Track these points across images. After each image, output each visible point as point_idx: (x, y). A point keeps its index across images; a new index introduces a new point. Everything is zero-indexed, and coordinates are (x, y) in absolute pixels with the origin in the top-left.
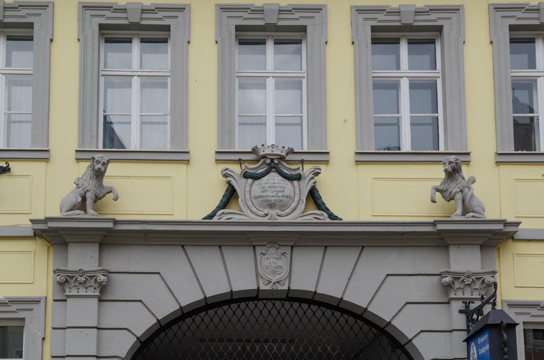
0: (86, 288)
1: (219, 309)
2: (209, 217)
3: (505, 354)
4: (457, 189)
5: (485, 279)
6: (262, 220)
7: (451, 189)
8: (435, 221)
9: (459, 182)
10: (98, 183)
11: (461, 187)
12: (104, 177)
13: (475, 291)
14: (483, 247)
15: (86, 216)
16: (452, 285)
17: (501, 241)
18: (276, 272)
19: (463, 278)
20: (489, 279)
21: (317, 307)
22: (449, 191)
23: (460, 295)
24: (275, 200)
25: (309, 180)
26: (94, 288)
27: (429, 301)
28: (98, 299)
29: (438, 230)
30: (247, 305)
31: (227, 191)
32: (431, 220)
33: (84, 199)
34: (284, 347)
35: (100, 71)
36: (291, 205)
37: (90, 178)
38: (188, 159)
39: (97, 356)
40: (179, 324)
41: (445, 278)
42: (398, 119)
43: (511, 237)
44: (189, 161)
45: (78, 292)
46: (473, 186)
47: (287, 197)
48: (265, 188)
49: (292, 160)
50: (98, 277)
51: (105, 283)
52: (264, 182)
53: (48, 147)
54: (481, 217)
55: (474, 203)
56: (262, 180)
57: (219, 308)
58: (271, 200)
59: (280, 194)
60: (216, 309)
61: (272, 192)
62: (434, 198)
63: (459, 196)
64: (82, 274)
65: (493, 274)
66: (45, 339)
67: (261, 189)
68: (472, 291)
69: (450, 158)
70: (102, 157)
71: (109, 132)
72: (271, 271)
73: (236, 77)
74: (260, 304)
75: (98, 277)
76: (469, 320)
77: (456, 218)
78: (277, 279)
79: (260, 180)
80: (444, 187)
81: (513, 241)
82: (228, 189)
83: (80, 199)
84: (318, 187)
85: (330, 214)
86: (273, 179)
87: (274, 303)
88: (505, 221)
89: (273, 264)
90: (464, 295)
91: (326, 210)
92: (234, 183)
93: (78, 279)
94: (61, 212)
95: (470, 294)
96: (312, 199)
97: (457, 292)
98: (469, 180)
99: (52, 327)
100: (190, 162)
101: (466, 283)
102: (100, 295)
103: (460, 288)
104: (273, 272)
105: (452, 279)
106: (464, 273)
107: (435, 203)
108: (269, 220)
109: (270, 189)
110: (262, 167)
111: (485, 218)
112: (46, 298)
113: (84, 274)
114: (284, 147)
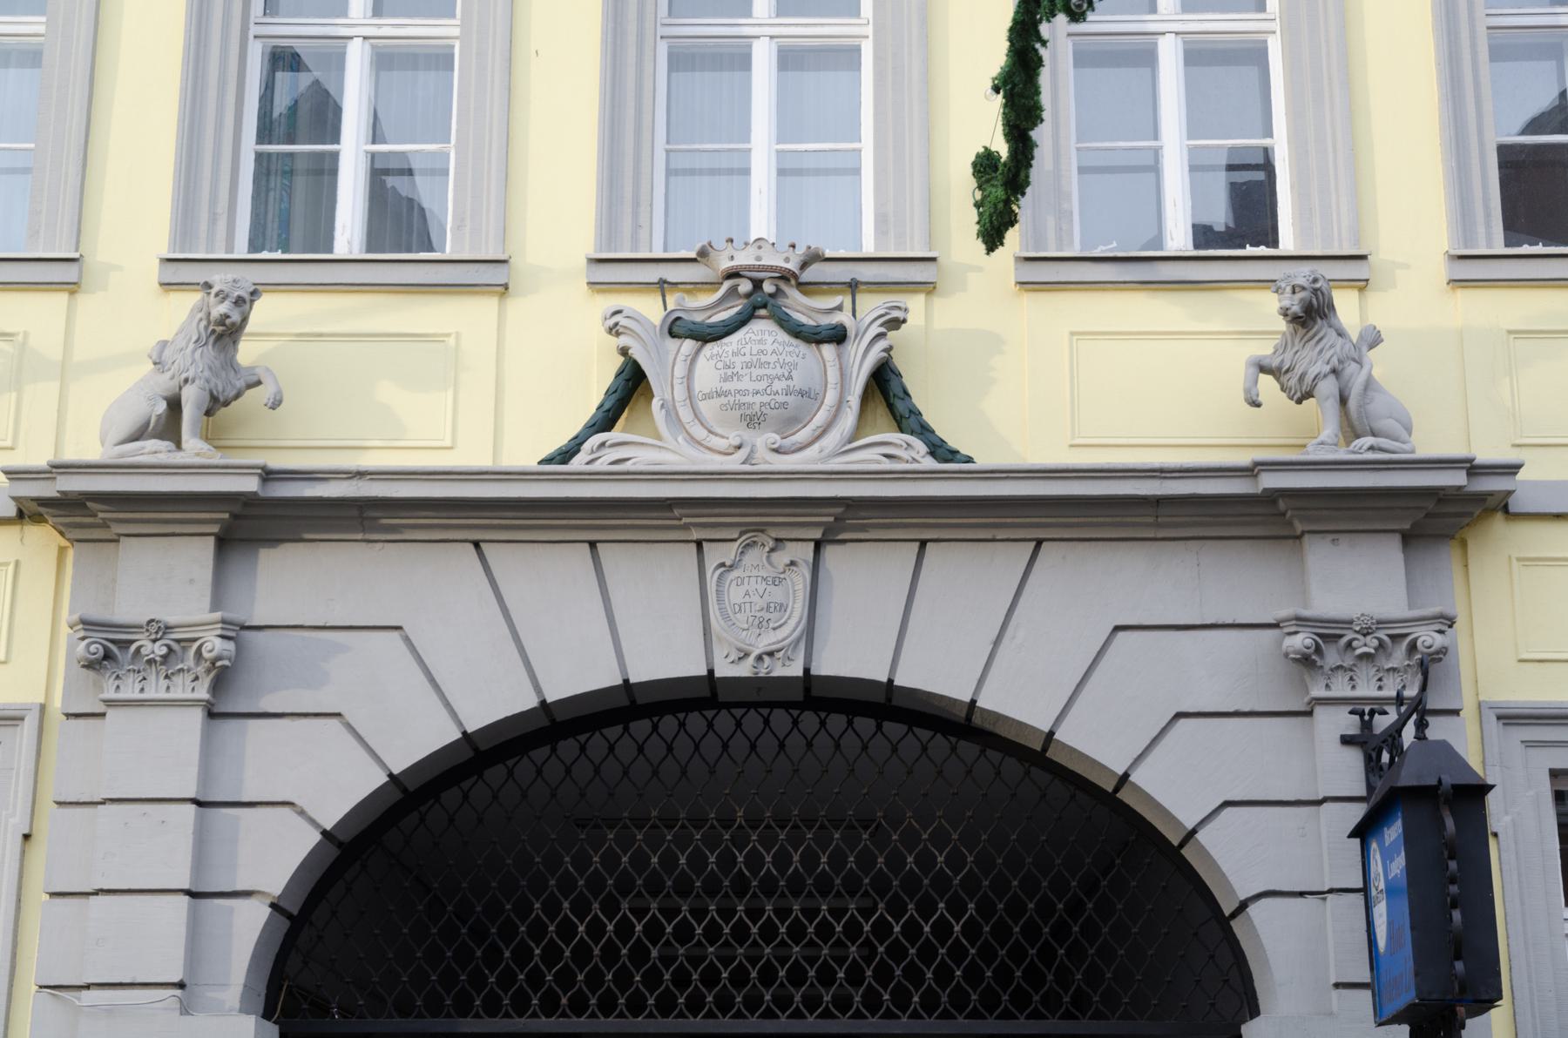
0: (167, 677)
1: (520, 759)
2: (560, 454)
3: (1453, 881)
4: (1321, 367)
5: (1416, 639)
6: (722, 464)
7: (1303, 366)
8: (1257, 464)
9: (1327, 346)
10: (222, 356)
11: (1335, 360)
12: (243, 338)
13: (1389, 675)
14: (1409, 539)
15: (178, 458)
16: (1314, 657)
17: (1466, 520)
18: (764, 623)
19: (1350, 635)
20: (1428, 637)
21: (904, 728)
22: (1298, 371)
23: (1341, 688)
24: (765, 405)
25: (870, 342)
26: (193, 676)
27: (1247, 709)
28: (207, 710)
29: (1265, 490)
30: (682, 725)
31: (617, 376)
32: (1243, 458)
33: (175, 405)
34: (796, 858)
35: (252, 26)
36: (812, 419)
37: (196, 341)
38: (503, 282)
39: (194, 890)
40: (466, 785)
41: (1293, 637)
42: (1157, 152)
43: (1501, 506)
44: (506, 287)
45: (142, 690)
46: (1372, 355)
47: (802, 393)
48: (732, 366)
49: (822, 281)
50: (205, 642)
51: (226, 663)
52: (729, 349)
53: (77, 250)
54: (1401, 448)
55: (1377, 406)
56: (726, 344)
57: (522, 757)
58: (750, 405)
59: (779, 385)
60: (582, 738)
61: (754, 378)
62: (1253, 393)
63: (1328, 387)
64: (157, 633)
65: (1440, 623)
66: (33, 838)
67: (722, 372)
68: (1381, 675)
69: (1295, 277)
70: (234, 281)
71: (277, 197)
72: (751, 619)
73: (662, 37)
74: (724, 721)
75: (205, 642)
76: (1372, 765)
77: (1317, 452)
78: (770, 645)
79: (718, 342)
80: (1282, 361)
81: (1507, 519)
82: (623, 372)
83: (162, 407)
84: (899, 362)
85: (934, 445)
86: (760, 341)
87: (766, 715)
88: (1470, 461)
89: (755, 599)
90: (1353, 687)
91: (924, 431)
92: (637, 354)
93: (142, 650)
94: (103, 445)
95: (1374, 683)
96: (883, 400)
97: (1333, 680)
98: (1361, 337)
99: (55, 800)
100: (510, 290)
101: (1358, 652)
102: (211, 699)
103: (1340, 667)
104: (757, 622)
105: (1314, 640)
106: (1351, 622)
107: (1257, 409)
108: (743, 463)
109: (748, 371)
110: (729, 305)
111: (1413, 452)
112: (43, 708)
113: (164, 633)
114: (793, 246)
